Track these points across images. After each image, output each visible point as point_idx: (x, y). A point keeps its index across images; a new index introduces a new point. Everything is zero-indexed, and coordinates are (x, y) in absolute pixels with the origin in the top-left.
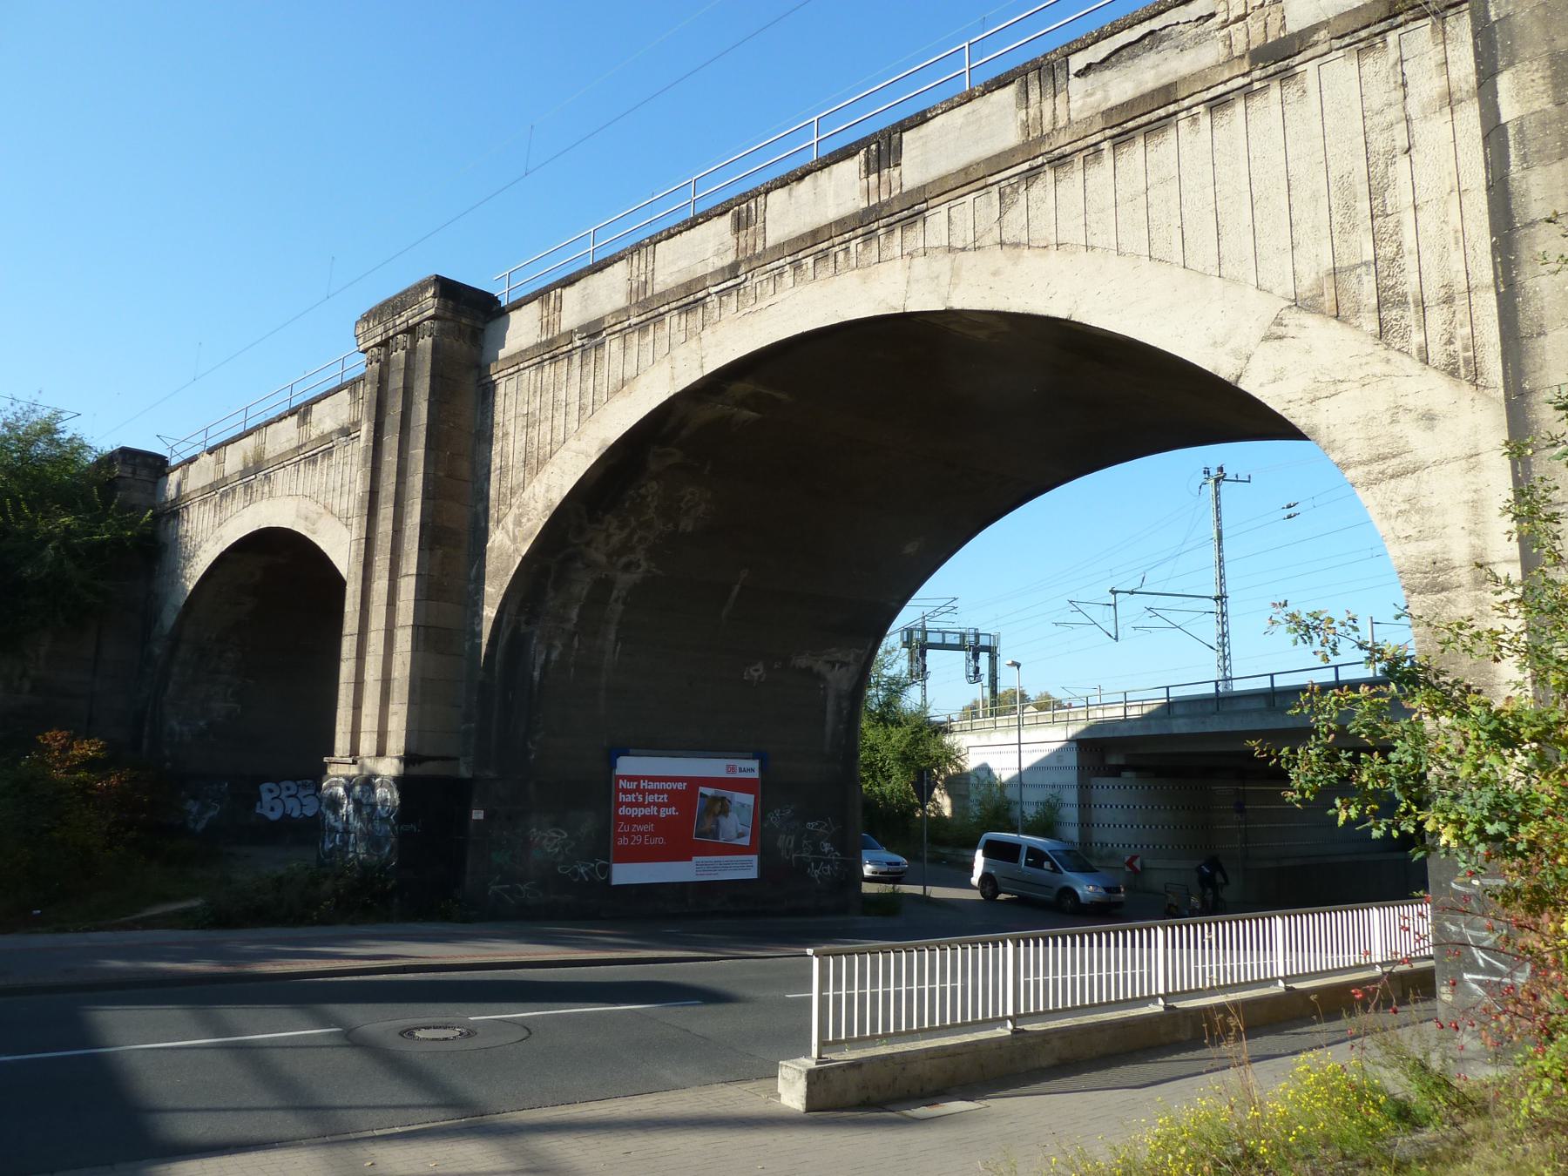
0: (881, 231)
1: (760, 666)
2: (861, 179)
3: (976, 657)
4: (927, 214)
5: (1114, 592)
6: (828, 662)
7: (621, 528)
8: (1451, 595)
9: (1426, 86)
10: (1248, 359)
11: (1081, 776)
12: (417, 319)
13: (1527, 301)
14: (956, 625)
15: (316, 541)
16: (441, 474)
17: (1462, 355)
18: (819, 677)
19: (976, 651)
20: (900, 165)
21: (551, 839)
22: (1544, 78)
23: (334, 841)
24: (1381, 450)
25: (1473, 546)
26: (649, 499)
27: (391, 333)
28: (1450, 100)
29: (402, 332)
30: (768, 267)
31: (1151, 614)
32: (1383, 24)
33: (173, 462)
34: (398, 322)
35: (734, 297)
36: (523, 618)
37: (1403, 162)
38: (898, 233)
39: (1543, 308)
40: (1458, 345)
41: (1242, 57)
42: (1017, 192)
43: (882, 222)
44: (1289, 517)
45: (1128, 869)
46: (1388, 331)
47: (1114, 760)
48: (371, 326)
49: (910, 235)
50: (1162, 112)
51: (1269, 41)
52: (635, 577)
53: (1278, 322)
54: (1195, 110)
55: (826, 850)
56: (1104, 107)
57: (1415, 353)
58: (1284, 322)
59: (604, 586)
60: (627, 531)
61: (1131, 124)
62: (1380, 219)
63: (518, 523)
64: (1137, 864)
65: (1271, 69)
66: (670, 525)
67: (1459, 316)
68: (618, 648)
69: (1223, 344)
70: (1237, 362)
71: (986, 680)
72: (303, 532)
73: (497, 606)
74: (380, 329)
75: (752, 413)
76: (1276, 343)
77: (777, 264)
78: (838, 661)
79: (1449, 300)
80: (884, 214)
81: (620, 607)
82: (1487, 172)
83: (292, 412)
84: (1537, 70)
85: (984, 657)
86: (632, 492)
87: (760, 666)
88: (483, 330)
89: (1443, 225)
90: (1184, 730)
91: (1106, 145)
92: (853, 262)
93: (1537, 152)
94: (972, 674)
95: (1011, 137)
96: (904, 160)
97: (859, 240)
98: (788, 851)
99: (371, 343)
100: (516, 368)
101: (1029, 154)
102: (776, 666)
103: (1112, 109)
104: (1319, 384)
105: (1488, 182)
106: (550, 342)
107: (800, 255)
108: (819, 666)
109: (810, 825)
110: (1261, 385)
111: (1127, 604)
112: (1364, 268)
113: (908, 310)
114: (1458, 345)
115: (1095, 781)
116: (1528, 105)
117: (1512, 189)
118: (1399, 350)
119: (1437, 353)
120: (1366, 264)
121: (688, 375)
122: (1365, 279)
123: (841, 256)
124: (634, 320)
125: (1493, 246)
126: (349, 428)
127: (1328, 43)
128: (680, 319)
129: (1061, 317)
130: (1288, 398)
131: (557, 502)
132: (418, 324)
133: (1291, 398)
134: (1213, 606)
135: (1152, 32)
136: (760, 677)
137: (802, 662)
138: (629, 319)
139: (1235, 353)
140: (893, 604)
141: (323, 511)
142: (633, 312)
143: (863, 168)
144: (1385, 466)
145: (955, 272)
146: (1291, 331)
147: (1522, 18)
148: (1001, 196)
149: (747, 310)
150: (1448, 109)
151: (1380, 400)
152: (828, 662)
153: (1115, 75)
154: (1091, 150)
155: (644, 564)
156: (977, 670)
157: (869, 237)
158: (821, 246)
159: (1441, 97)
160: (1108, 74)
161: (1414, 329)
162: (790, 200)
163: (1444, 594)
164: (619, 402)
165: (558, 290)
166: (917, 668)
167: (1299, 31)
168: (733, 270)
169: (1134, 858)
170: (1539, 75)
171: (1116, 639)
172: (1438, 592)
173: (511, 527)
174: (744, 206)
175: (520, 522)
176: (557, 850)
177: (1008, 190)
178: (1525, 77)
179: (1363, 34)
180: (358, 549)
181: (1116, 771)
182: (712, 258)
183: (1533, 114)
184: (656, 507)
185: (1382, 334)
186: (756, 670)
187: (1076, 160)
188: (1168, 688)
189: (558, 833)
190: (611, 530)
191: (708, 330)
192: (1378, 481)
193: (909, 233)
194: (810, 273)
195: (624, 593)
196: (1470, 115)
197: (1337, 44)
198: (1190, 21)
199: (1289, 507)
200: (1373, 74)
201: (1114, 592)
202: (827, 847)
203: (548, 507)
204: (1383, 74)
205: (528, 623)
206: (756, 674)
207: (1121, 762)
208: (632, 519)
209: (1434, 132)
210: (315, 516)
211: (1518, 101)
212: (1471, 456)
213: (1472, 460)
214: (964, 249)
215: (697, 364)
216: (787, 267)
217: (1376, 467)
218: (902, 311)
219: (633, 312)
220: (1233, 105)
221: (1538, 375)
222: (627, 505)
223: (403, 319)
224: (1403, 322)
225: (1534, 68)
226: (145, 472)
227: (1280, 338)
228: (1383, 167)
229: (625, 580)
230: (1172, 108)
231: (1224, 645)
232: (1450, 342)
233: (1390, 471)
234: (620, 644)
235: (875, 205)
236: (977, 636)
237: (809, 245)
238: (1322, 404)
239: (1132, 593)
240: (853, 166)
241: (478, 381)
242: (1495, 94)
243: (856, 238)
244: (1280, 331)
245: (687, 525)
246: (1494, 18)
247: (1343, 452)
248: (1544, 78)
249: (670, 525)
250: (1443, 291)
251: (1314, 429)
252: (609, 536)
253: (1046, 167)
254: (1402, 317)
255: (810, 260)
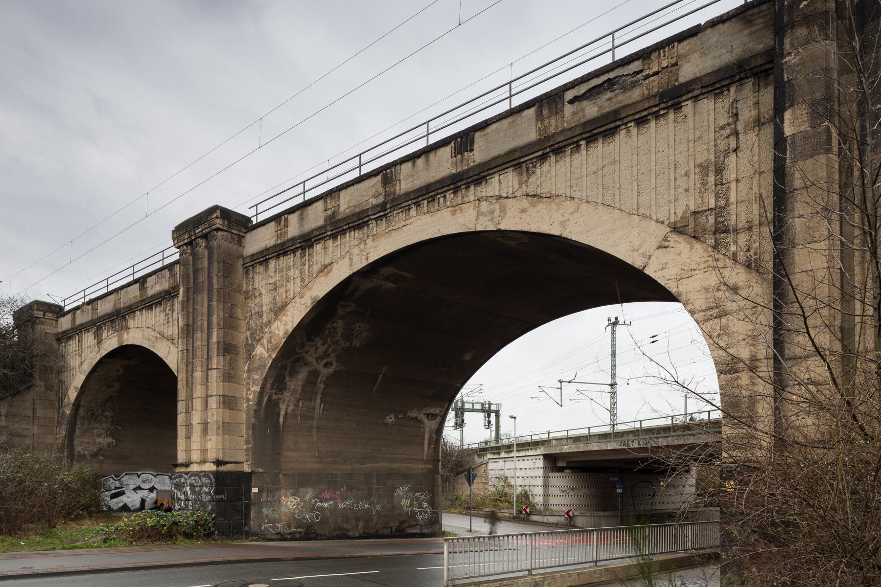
0: (463, 187)
1: (392, 416)
2: (452, 158)
3: (489, 415)
4: (487, 178)
5: (560, 381)
6: (425, 414)
7: (323, 344)
8: (740, 374)
9: (747, 114)
10: (649, 258)
11: (544, 472)
12: (208, 230)
13: (788, 230)
14: (482, 398)
15: (155, 352)
16: (227, 315)
17: (754, 257)
18: (421, 422)
19: (488, 412)
20: (473, 150)
21: (291, 502)
22: (807, 113)
23: (180, 505)
24: (711, 304)
25: (751, 351)
26: (338, 329)
27: (193, 238)
28: (758, 123)
29: (199, 237)
30: (402, 205)
31: (578, 393)
32: (728, 80)
33: (67, 308)
34: (197, 231)
35: (384, 221)
36: (274, 391)
37: (733, 157)
38: (472, 188)
39: (795, 234)
40: (752, 252)
41: (655, 96)
42: (535, 167)
43: (464, 182)
44: (653, 342)
45: (566, 516)
46: (719, 244)
47: (561, 464)
48: (181, 233)
49: (479, 189)
50: (612, 125)
51: (669, 88)
52: (331, 370)
53: (665, 239)
54: (629, 125)
55: (425, 506)
56: (582, 121)
57: (731, 255)
58: (669, 239)
59: (315, 374)
60: (326, 346)
61: (596, 131)
62: (719, 186)
63: (270, 341)
64: (571, 514)
65: (670, 103)
66: (348, 343)
67: (754, 237)
68: (322, 406)
69: (637, 250)
70: (643, 259)
71: (493, 428)
72: (148, 347)
73: (260, 385)
74: (187, 236)
75: (392, 284)
76: (663, 250)
77: (406, 204)
78: (430, 414)
79: (750, 229)
80: (464, 177)
81: (322, 386)
82: (774, 163)
83: (135, 282)
84: (804, 109)
85: (493, 415)
86: (329, 326)
87: (392, 416)
88: (244, 237)
89: (750, 190)
90: (596, 448)
91: (583, 143)
92: (448, 203)
93: (799, 153)
94: (487, 424)
95: (532, 136)
96: (476, 147)
97: (451, 192)
98: (407, 507)
99: (182, 243)
100: (264, 258)
101: (542, 146)
102: (400, 416)
103: (587, 122)
104: (683, 271)
105: (774, 168)
106: (283, 244)
107: (420, 199)
108: (421, 417)
109: (417, 494)
110: (655, 271)
111: (567, 388)
112: (709, 212)
113: (477, 230)
114: (752, 252)
115: (551, 474)
116: (798, 128)
117: (787, 172)
118: (724, 254)
119: (742, 258)
120: (711, 209)
121: (359, 264)
122: (710, 217)
123: (442, 200)
124: (329, 233)
125: (774, 201)
126: (170, 291)
127: (700, 90)
128: (355, 233)
129: (556, 234)
130: (668, 278)
131: (290, 331)
132: (209, 233)
133: (670, 278)
134: (609, 388)
135: (609, 80)
136: (392, 422)
137: (413, 414)
138: (326, 232)
139: (643, 255)
140: (458, 385)
141: (158, 335)
142: (329, 228)
143: (453, 151)
144: (713, 312)
145: (503, 210)
146: (672, 244)
147: (800, 80)
148: (528, 169)
149: (391, 228)
150: (757, 128)
151: (712, 279)
152: (425, 414)
153: (589, 103)
154: (575, 145)
155: (335, 364)
156: (489, 422)
157: (456, 191)
158: (431, 194)
159: (754, 121)
160: (585, 103)
161: (732, 244)
162: (414, 168)
163: (736, 374)
164: (322, 279)
165: (286, 216)
166: (459, 421)
167: (686, 82)
168: (383, 206)
169: (569, 511)
170: (805, 112)
171: (561, 406)
172: (734, 373)
173: (265, 343)
174: (388, 170)
175: (271, 341)
176: (295, 507)
177: (531, 166)
178: (798, 112)
179: (718, 85)
180: (183, 355)
181: (561, 470)
182: (371, 200)
183: (800, 132)
184: (341, 334)
185: (715, 247)
186: (391, 418)
187: (567, 150)
188: (589, 428)
189: (295, 499)
190: (318, 345)
191: (370, 239)
192: (709, 320)
193: (478, 188)
194: (425, 209)
195: (324, 379)
196: (768, 132)
197: (704, 91)
198: (629, 74)
199: (653, 337)
200: (721, 108)
201: (560, 381)
202: (425, 505)
203: (286, 333)
204: (726, 108)
205: (276, 394)
206: (390, 420)
207: (565, 465)
208: (329, 340)
209: (749, 139)
210: (154, 339)
211: (793, 126)
212: (754, 308)
213: (754, 309)
214: (507, 197)
215: (364, 257)
216: (413, 206)
217: (709, 313)
218: (474, 230)
219: (329, 228)
220: (649, 123)
221: (790, 267)
222: (326, 332)
223: (200, 230)
224: (726, 240)
225: (803, 108)
226: (50, 315)
227: (666, 247)
228: (722, 158)
229: (325, 372)
230: (617, 123)
231: (614, 408)
232: (748, 250)
233: (715, 315)
234: (322, 405)
235: (460, 172)
236: (490, 404)
237: (424, 193)
238: (685, 281)
239: (570, 382)
240: (447, 151)
241: (243, 265)
242: (782, 121)
243: (449, 190)
244: (665, 244)
245: (356, 343)
246: (786, 80)
247: (693, 305)
248: (807, 113)
249: (348, 343)
250: (747, 224)
251: (680, 294)
252: (317, 349)
253: (551, 154)
254: (726, 237)
255: (426, 202)
